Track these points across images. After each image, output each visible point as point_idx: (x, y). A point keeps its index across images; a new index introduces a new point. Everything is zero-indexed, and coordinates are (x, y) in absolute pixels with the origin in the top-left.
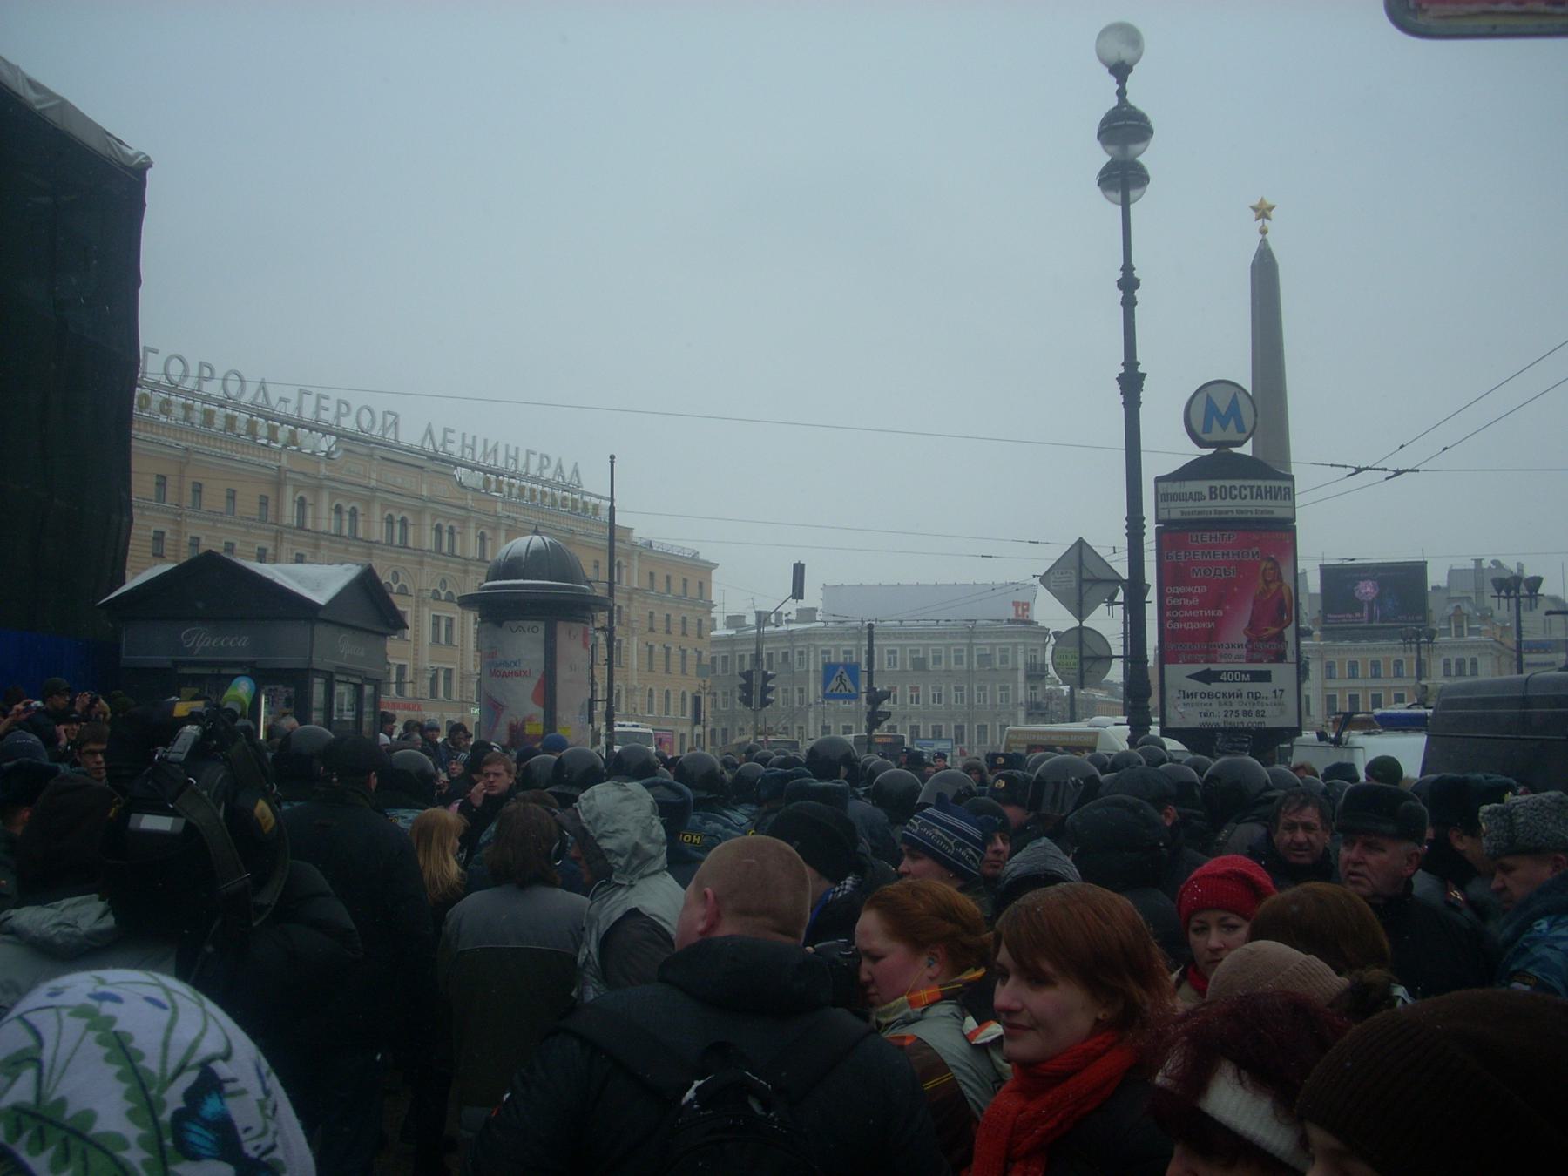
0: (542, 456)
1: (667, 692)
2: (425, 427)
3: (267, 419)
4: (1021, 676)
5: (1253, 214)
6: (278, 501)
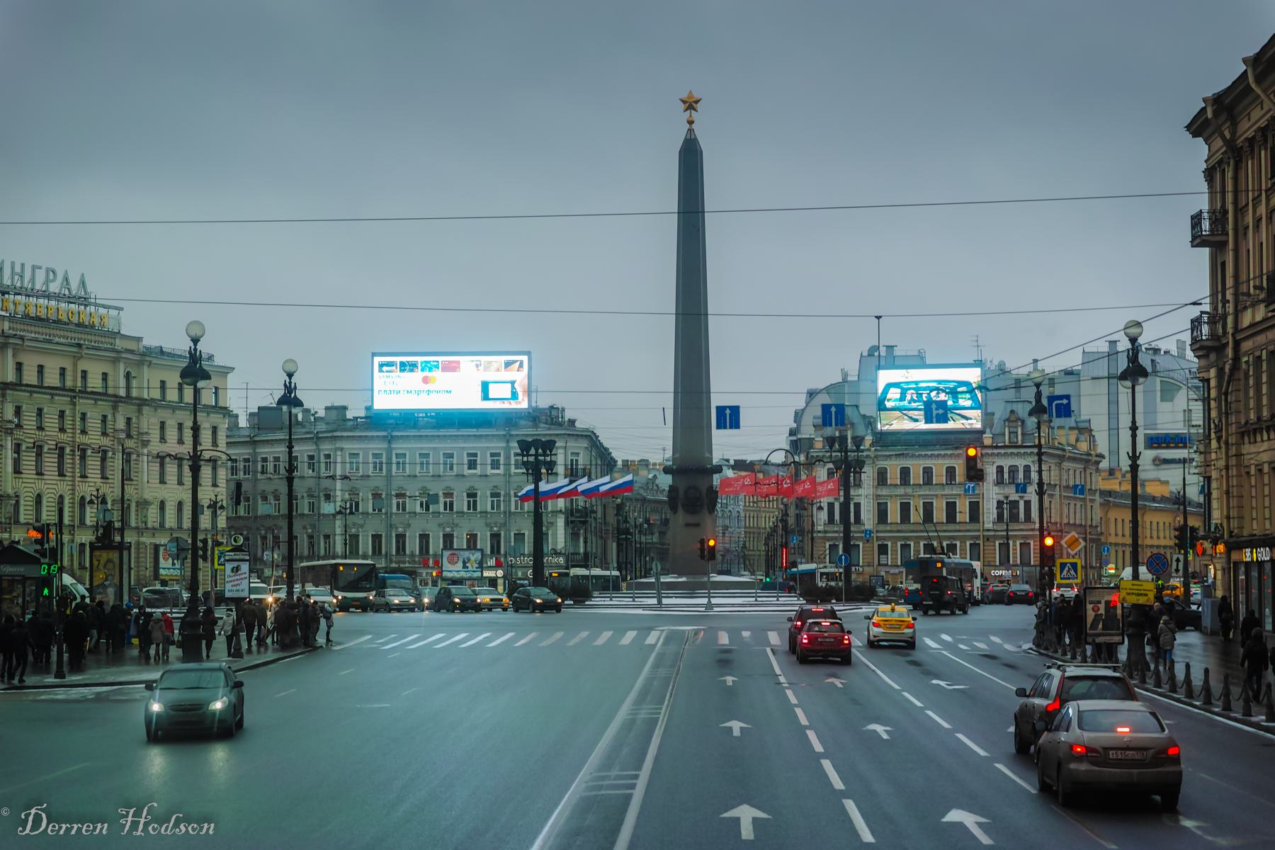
0: (48, 270)
1: (39, 497)
5: (682, 106)
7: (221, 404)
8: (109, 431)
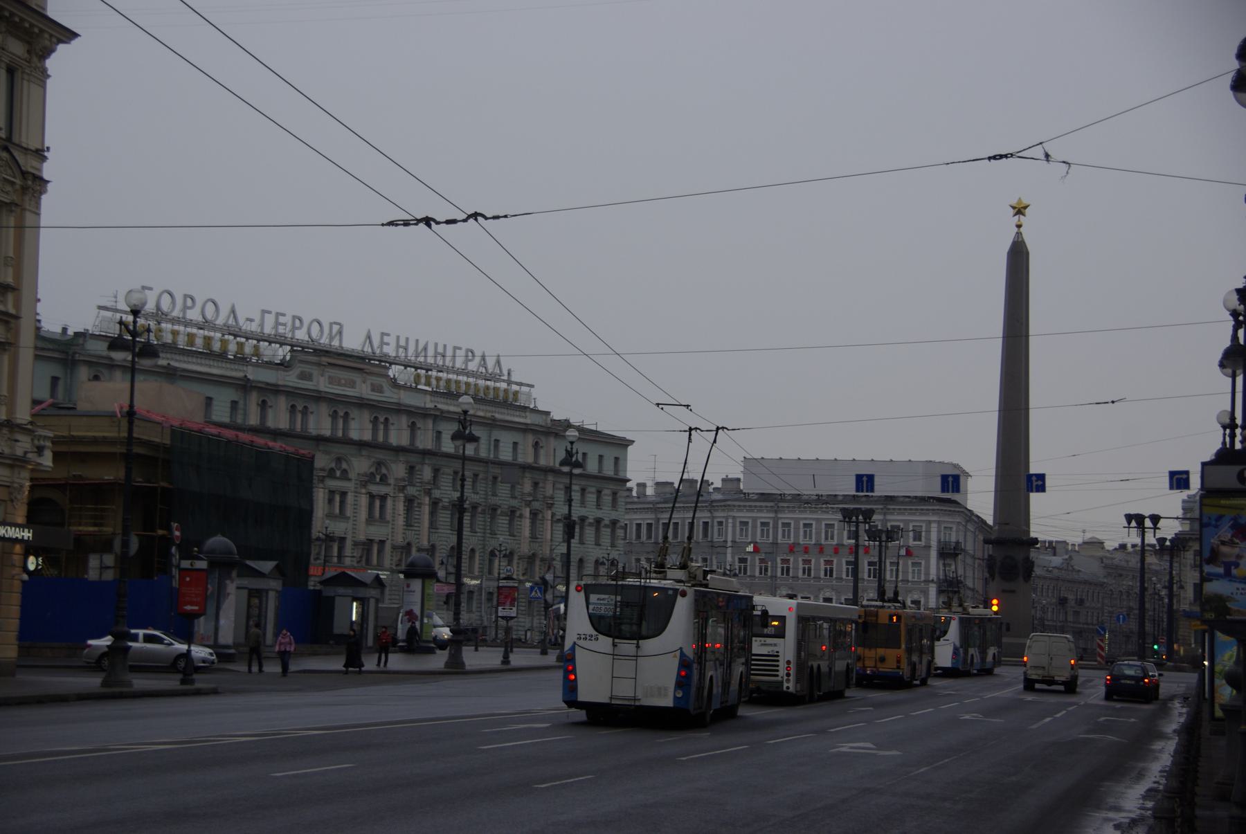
0: (468, 350)
2: (364, 334)
3: (236, 336)
4: (934, 554)
5: (1012, 212)
6: (245, 405)
7: (621, 475)
8: (517, 494)
